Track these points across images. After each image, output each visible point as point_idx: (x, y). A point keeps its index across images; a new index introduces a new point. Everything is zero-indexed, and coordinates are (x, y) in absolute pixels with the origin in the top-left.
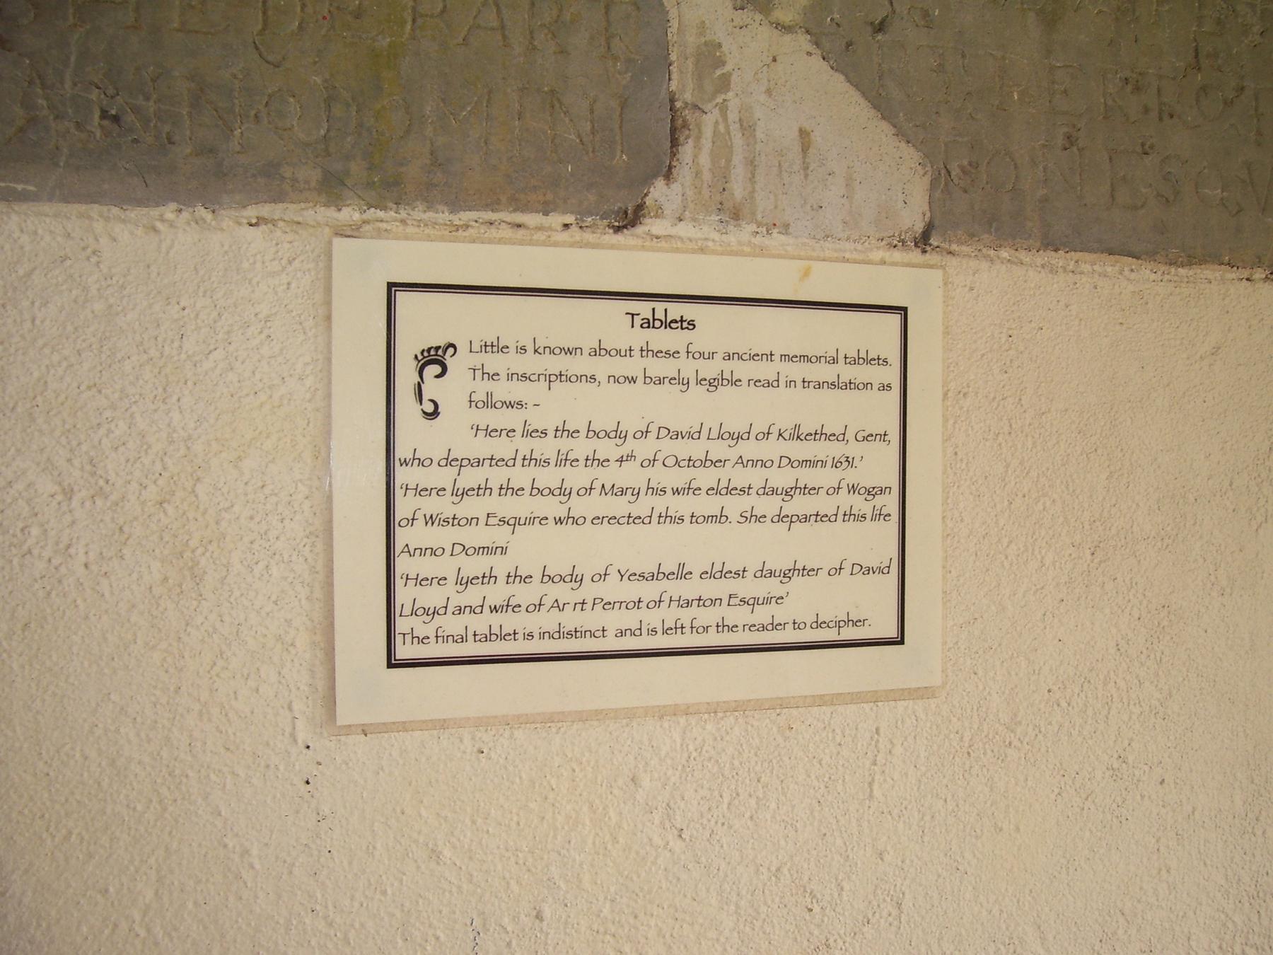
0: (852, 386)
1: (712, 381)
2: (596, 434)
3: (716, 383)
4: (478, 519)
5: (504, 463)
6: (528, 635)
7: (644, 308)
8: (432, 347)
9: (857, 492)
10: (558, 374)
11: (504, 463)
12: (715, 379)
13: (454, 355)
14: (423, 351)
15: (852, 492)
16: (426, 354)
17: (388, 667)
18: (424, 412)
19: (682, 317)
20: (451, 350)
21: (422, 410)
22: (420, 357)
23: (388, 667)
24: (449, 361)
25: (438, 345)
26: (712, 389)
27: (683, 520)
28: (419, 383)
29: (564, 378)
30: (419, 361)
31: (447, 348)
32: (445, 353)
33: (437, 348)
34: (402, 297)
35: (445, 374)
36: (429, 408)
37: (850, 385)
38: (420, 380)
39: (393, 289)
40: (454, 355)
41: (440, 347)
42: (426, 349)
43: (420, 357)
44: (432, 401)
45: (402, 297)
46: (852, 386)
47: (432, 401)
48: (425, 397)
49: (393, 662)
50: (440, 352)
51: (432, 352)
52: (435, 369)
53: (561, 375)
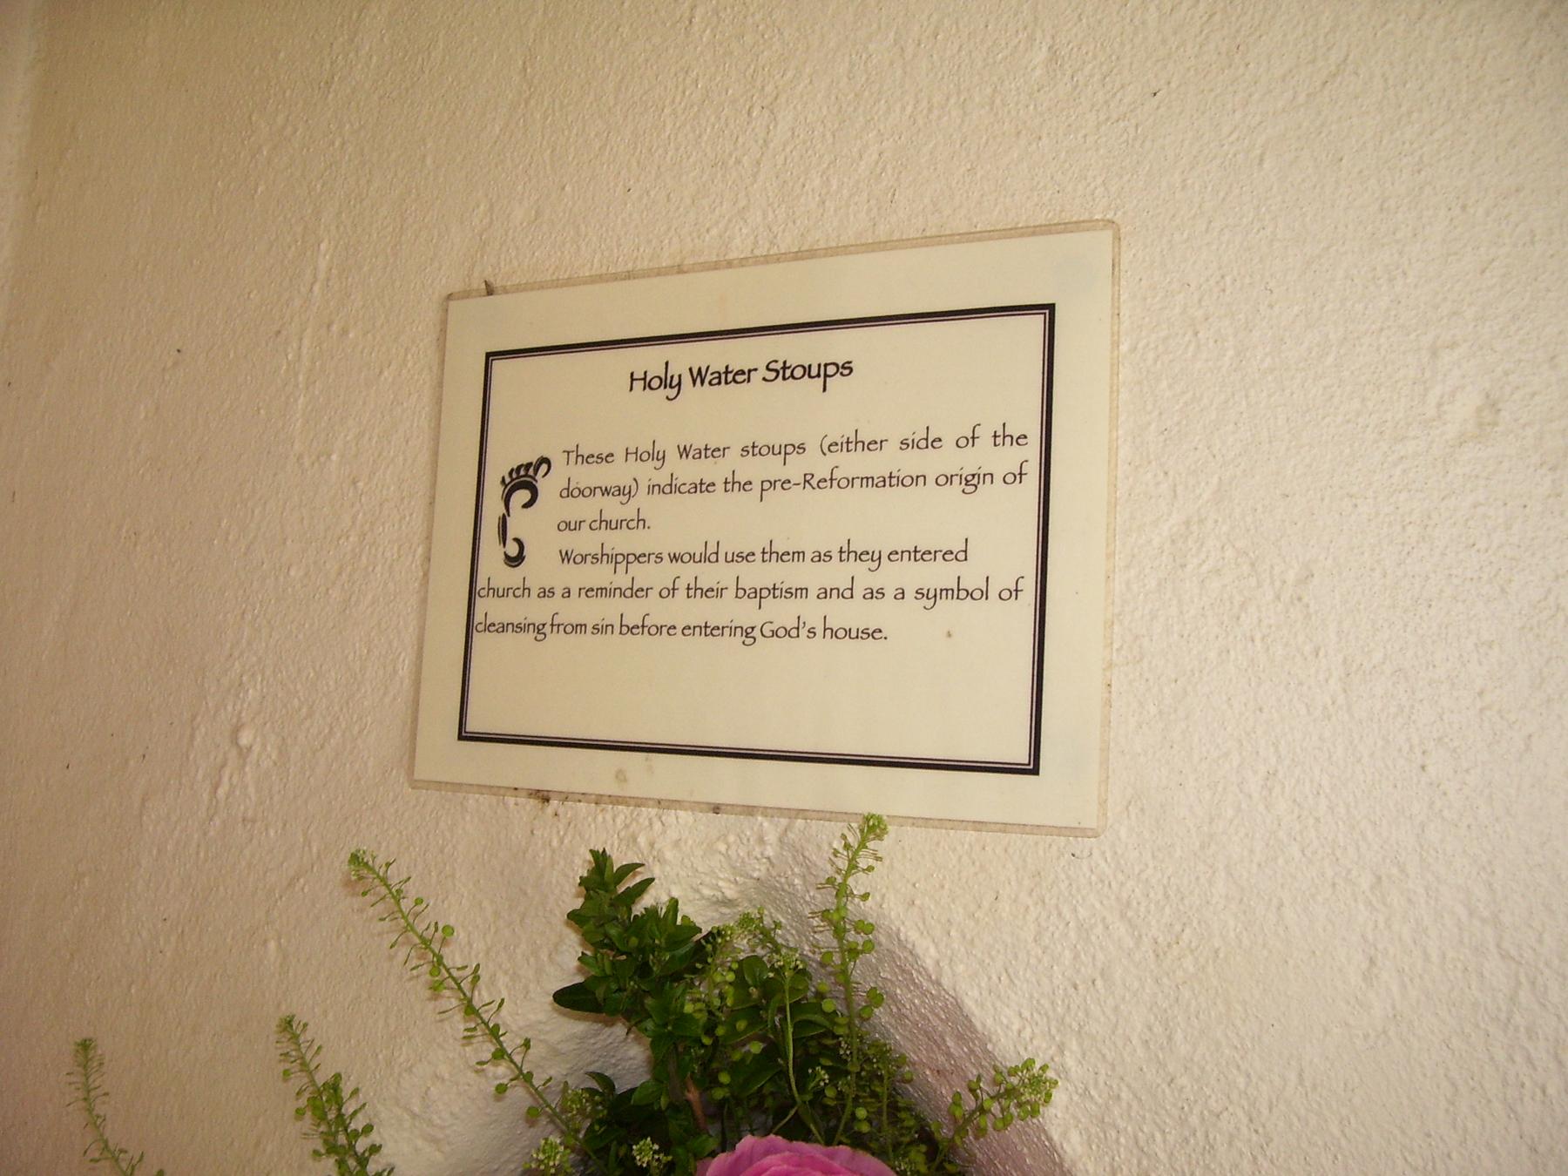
0: (894, 481)
1: (970, 478)
2: (834, 634)
3: (975, 481)
4: (992, 475)
5: (953, 556)
6: (786, 592)
7: (650, 360)
8: (522, 465)
9: (571, 561)
10: (771, 587)
11: (953, 556)
12: (973, 476)
13: (546, 474)
14: (512, 470)
15: (566, 560)
16: (514, 476)
17: (1053, 305)
18: (507, 556)
19: (727, 367)
20: (544, 467)
21: (505, 554)
22: (508, 480)
23: (1053, 305)
24: (542, 484)
25: (529, 461)
26: (970, 489)
27: (815, 634)
28: (504, 515)
29: (778, 593)
30: (506, 486)
31: (541, 464)
32: (536, 471)
33: (528, 465)
34: (1021, 756)
35: (535, 501)
36: (513, 550)
37: (889, 481)
38: (505, 511)
39: (1031, 767)
40: (546, 474)
41: (531, 464)
42: (515, 467)
43: (508, 480)
44: (517, 540)
45: (1021, 756)
46: (894, 481)
47: (517, 540)
48: (510, 535)
49: (1047, 311)
50: (531, 472)
51: (522, 473)
52: (523, 496)
53: (774, 589)
